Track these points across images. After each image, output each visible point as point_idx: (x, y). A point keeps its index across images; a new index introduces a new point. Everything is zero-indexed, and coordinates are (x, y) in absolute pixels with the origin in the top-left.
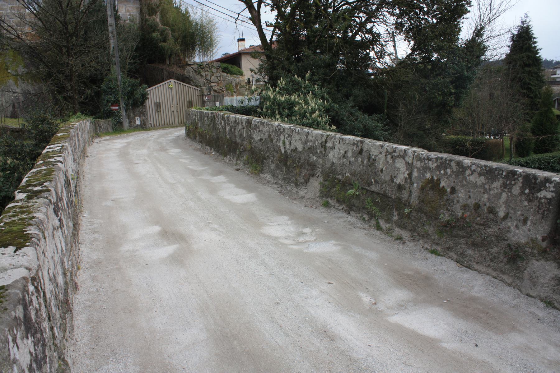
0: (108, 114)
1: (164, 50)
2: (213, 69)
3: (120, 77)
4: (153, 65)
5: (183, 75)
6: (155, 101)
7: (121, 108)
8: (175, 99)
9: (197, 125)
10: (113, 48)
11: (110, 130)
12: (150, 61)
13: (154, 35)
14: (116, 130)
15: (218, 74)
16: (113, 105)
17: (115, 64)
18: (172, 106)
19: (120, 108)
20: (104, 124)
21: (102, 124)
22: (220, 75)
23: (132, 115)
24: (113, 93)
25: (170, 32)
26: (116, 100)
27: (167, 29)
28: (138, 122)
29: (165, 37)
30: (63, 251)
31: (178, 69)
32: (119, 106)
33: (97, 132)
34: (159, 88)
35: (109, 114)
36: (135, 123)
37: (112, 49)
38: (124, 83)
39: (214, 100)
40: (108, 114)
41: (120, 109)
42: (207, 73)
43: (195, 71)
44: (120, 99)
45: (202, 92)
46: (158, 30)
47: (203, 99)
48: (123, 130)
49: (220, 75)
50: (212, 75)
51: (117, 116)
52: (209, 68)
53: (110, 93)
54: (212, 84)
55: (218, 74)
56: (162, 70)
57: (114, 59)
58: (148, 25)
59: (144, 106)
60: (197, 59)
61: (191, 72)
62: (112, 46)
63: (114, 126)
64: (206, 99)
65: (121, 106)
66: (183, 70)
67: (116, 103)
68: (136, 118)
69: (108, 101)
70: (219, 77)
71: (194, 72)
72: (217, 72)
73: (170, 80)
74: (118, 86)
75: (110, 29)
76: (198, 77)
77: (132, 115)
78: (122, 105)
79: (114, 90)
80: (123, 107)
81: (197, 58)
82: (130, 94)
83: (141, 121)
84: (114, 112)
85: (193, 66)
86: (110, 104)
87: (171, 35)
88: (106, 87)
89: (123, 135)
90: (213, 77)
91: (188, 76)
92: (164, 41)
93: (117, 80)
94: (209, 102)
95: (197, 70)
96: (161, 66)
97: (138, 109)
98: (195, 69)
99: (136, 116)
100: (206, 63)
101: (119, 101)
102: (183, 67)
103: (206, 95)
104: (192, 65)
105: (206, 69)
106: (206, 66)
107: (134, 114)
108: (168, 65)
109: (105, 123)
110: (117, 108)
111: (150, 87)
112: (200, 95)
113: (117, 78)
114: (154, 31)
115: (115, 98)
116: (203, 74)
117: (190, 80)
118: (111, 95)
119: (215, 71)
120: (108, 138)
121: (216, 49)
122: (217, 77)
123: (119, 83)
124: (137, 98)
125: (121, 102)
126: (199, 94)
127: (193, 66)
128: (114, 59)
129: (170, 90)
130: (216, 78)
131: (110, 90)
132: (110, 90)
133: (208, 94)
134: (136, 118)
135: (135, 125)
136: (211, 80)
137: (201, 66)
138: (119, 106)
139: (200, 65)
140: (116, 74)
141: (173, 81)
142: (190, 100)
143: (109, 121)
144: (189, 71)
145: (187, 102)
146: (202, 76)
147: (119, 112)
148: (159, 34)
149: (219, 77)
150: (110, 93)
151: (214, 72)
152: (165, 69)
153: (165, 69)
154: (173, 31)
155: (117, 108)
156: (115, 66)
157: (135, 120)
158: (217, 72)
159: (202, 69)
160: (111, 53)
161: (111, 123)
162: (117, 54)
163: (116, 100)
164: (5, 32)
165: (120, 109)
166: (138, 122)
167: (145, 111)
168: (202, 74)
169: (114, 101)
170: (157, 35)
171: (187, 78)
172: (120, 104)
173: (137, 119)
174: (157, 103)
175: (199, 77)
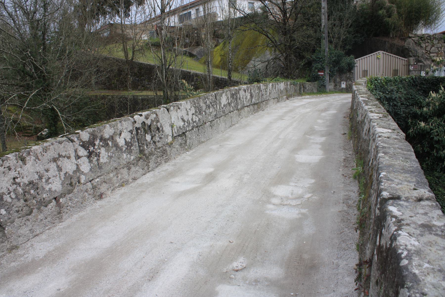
0: (316, 78)
1: (388, 25)
2: (434, 40)
3: (327, 49)
4: (377, 38)
5: (403, 47)
6: (363, 69)
7: (326, 74)
8: (381, 68)
9: (36, 95)
10: (324, 25)
11: (315, 91)
12: (376, 35)
13: (380, 12)
14: (320, 91)
15: (439, 45)
16: (319, 71)
17: (324, 39)
18: (378, 73)
19: (325, 74)
20: (310, 86)
21: (307, 86)
22: (441, 46)
23: (338, 80)
24: (321, 62)
25: (395, 9)
26: (323, 67)
27: (393, 6)
28: (343, 86)
29: (390, 14)
30: (232, 175)
31: (400, 41)
32: (324, 72)
33: (301, 91)
34: (373, 56)
35: (315, 79)
36: (340, 86)
37: (323, 27)
38: (331, 54)
39: (420, 69)
40: (316, 78)
41: (325, 74)
42: (427, 44)
43: (416, 43)
44: (325, 66)
45: (409, 62)
46: (385, 8)
47: (409, 68)
48: (325, 91)
49: (441, 46)
50: (433, 46)
51: (322, 80)
52: (430, 40)
53: (318, 62)
54: (432, 55)
55: (439, 45)
56: (385, 42)
57: (324, 35)
58: (377, 4)
59: (352, 73)
60: (419, 33)
61: (411, 44)
62: (323, 24)
63: (318, 88)
64: (411, 68)
65: (326, 73)
66: (404, 42)
67: (322, 70)
68: (342, 82)
69: (316, 68)
70: (439, 48)
71: (414, 43)
72: (438, 43)
73: (379, 51)
74: (325, 56)
75: (323, 10)
76: (417, 48)
77: (338, 80)
78: (327, 71)
79: (321, 60)
80: (327, 73)
81: (422, 31)
82: (336, 63)
83: (346, 85)
84: (320, 77)
85: (414, 39)
86: (317, 70)
87: (396, 13)
88: (316, 57)
89: (324, 95)
90: (433, 48)
91: (407, 48)
92: (390, 16)
93: (324, 51)
94: (415, 71)
95: (417, 42)
96: (386, 39)
97: (345, 75)
98: (416, 41)
99: (343, 81)
100: (427, 36)
101: (324, 68)
102: (404, 40)
103: (412, 65)
104: (413, 37)
105: (426, 41)
106: (427, 38)
107: (340, 79)
108: (391, 38)
109: (311, 85)
110: (322, 74)
111: (356, 58)
112: (406, 65)
113: (324, 50)
114: (381, 9)
115: (321, 65)
116: (423, 45)
117: (409, 51)
118: (319, 63)
119: (437, 42)
120: (308, 97)
121: (441, 22)
122: (438, 48)
123: (326, 54)
124: (342, 66)
125: (326, 69)
126: (405, 64)
127: (414, 39)
128: (324, 35)
129: (378, 60)
130: (436, 49)
131: (318, 59)
132: (318, 59)
133: (414, 64)
134: (342, 82)
135: (340, 88)
136: (431, 51)
137: (421, 38)
138: (324, 72)
139: (422, 38)
140: (324, 47)
141: (381, 52)
142: (396, 69)
143: (314, 84)
144: (410, 43)
145: (393, 70)
146: (421, 47)
147: (323, 77)
148: (385, 11)
149: (439, 48)
150: (318, 62)
151: (435, 43)
152: (388, 42)
153: (388, 42)
154: (399, 7)
155: (322, 74)
156: (324, 41)
157: (341, 84)
158: (438, 43)
159: (422, 40)
160: (322, 30)
161: (316, 86)
162: (326, 32)
163: (323, 67)
164: (167, 21)
165: (325, 74)
166: (343, 86)
167: (353, 77)
168: (422, 45)
169: (321, 68)
170: (384, 12)
171: (406, 49)
172: (325, 70)
173: (343, 83)
174: (365, 70)
175: (419, 48)
